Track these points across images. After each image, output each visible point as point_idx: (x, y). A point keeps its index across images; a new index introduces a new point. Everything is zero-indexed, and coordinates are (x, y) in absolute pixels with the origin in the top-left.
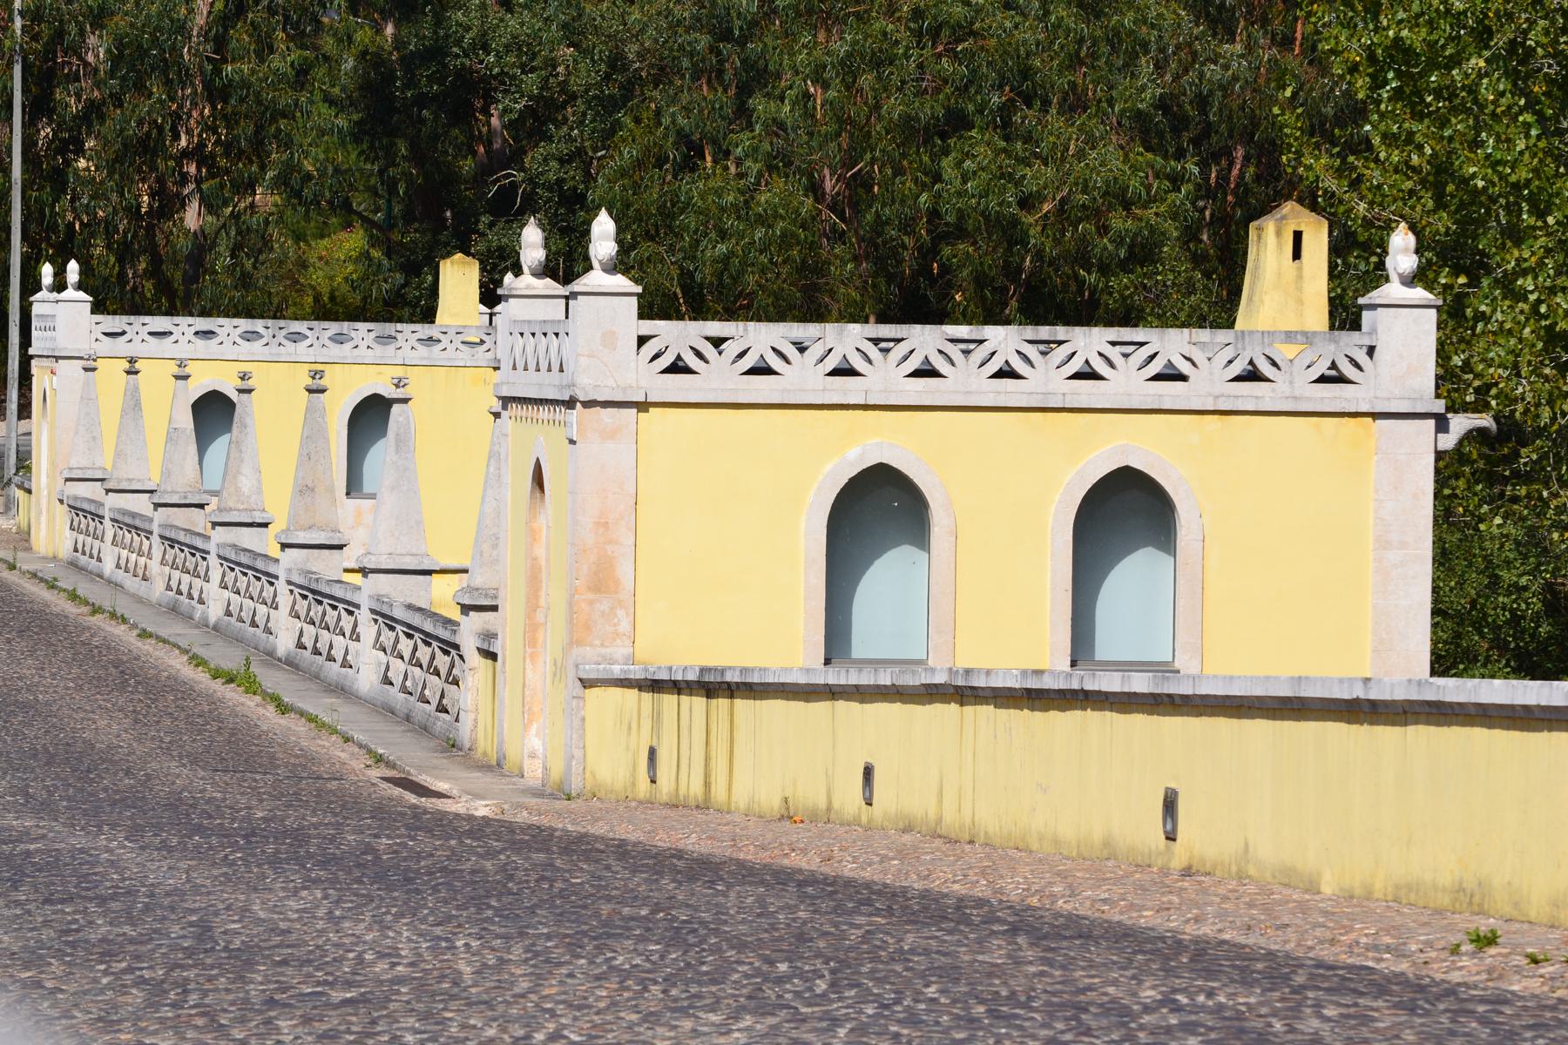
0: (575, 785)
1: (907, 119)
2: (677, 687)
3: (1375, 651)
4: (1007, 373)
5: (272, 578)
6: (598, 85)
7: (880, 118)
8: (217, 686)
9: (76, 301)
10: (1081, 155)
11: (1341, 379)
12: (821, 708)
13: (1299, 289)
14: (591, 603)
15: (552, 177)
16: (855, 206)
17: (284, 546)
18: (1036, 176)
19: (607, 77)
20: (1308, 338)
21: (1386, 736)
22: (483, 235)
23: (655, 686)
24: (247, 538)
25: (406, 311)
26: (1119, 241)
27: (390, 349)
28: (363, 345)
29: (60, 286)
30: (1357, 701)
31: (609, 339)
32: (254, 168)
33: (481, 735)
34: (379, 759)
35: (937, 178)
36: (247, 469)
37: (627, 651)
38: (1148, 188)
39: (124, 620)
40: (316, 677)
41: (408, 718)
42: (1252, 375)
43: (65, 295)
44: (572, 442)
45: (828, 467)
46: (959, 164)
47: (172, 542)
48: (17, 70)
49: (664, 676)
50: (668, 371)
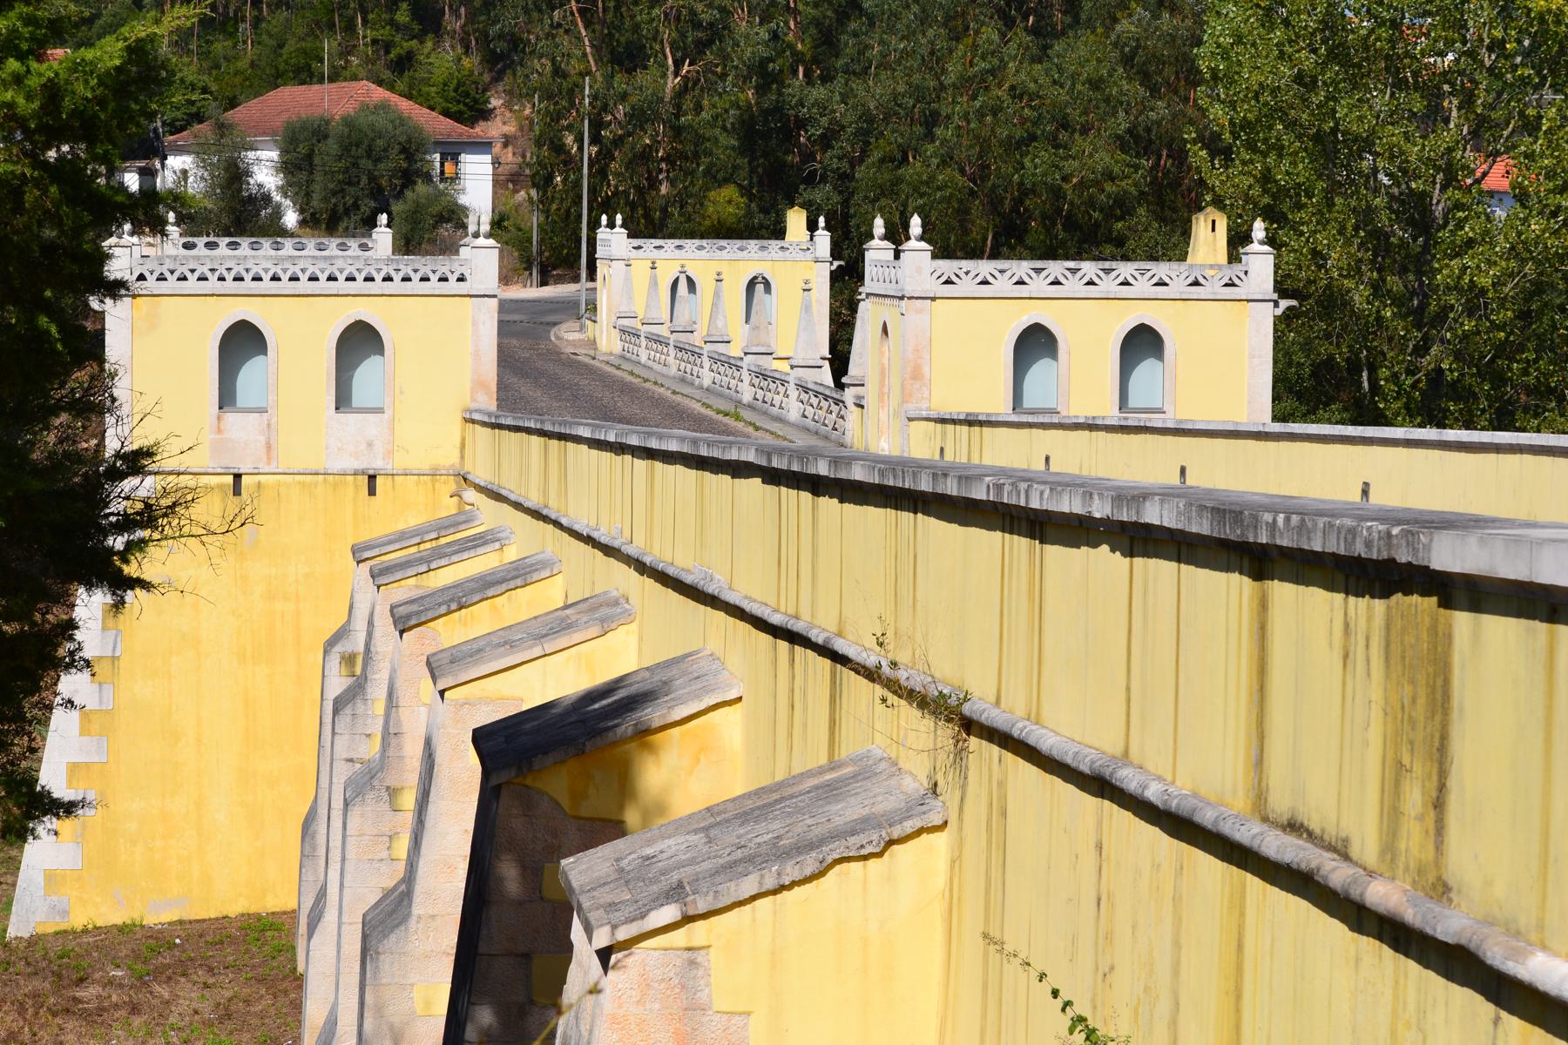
1: (1009, 137)
2: (954, 422)
3: (1249, 402)
4: (1091, 283)
5: (639, 336)
7: (995, 137)
8: (720, 417)
9: (620, 232)
10: (1091, 155)
11: (1233, 285)
12: (1025, 431)
13: (1215, 245)
14: (912, 384)
16: (983, 181)
17: (672, 332)
18: (1070, 165)
20: (1220, 267)
21: (1271, 445)
22: (801, 194)
23: (943, 421)
24: (721, 348)
25: (763, 232)
26: (1109, 196)
27: (766, 253)
28: (753, 251)
29: (611, 225)
30: (1260, 432)
31: (919, 270)
32: (694, 165)
33: (856, 442)
35: (1023, 168)
36: (720, 317)
38: (1123, 172)
39: (662, 386)
40: (765, 413)
41: (816, 433)
42: (1196, 283)
43: (614, 230)
44: (902, 314)
45: (1014, 324)
46: (1033, 160)
47: (681, 349)
48: (586, 122)
49: (948, 417)
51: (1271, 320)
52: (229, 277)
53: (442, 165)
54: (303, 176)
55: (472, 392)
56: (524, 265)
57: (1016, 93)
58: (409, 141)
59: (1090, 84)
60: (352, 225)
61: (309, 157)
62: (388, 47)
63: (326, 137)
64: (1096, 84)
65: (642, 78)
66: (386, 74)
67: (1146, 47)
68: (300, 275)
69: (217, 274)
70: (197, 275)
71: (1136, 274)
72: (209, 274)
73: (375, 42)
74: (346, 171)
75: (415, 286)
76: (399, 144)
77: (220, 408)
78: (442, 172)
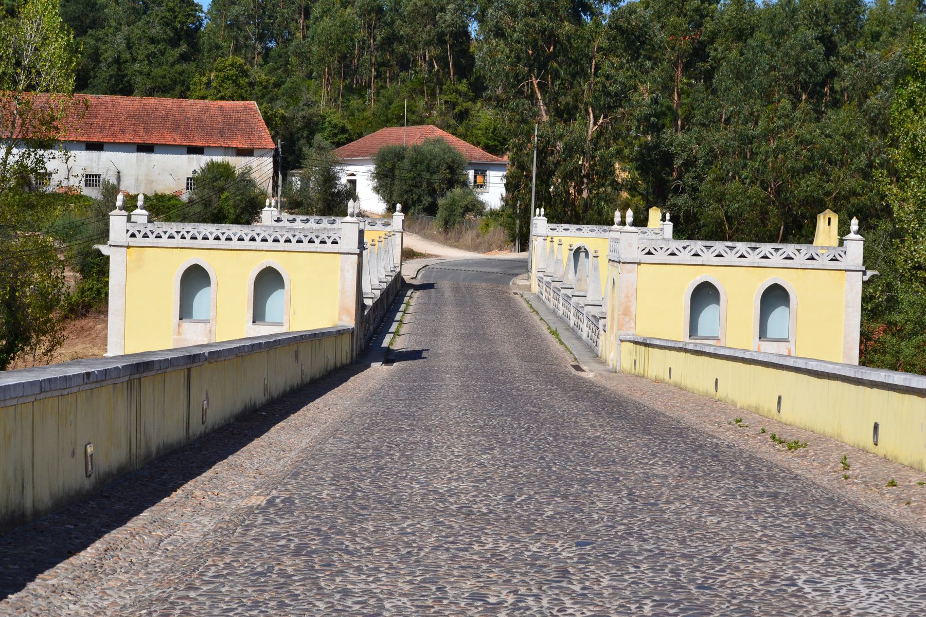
0: (618, 369)
6: (705, 156)
15: (690, 183)
19: (708, 154)
23: (636, 343)
26: (853, 206)
34: (576, 359)
37: (633, 332)
39: (538, 314)
42: (812, 258)
48: (535, 152)
50: (647, 254)
51: (861, 283)
52: (188, 236)
53: (475, 177)
54: (389, 181)
55: (339, 314)
56: (511, 239)
57: (800, 141)
58: (453, 162)
59: (845, 137)
60: (416, 212)
61: (392, 170)
62: (454, 105)
63: (403, 158)
64: (848, 136)
65: (576, 125)
66: (453, 122)
67: (884, 114)
68: (233, 237)
69: (180, 234)
70: (168, 234)
71: (772, 251)
72: (175, 235)
73: (446, 102)
74: (414, 179)
75: (223, 243)
76: (447, 163)
77: (180, 319)
78: (475, 182)
